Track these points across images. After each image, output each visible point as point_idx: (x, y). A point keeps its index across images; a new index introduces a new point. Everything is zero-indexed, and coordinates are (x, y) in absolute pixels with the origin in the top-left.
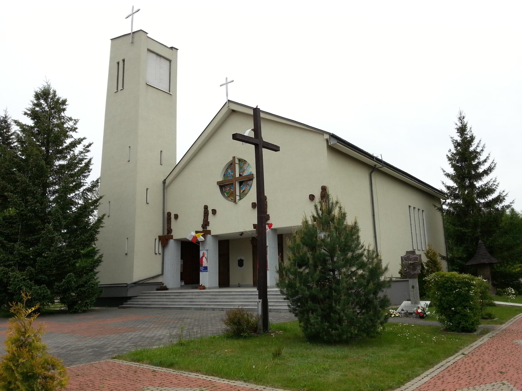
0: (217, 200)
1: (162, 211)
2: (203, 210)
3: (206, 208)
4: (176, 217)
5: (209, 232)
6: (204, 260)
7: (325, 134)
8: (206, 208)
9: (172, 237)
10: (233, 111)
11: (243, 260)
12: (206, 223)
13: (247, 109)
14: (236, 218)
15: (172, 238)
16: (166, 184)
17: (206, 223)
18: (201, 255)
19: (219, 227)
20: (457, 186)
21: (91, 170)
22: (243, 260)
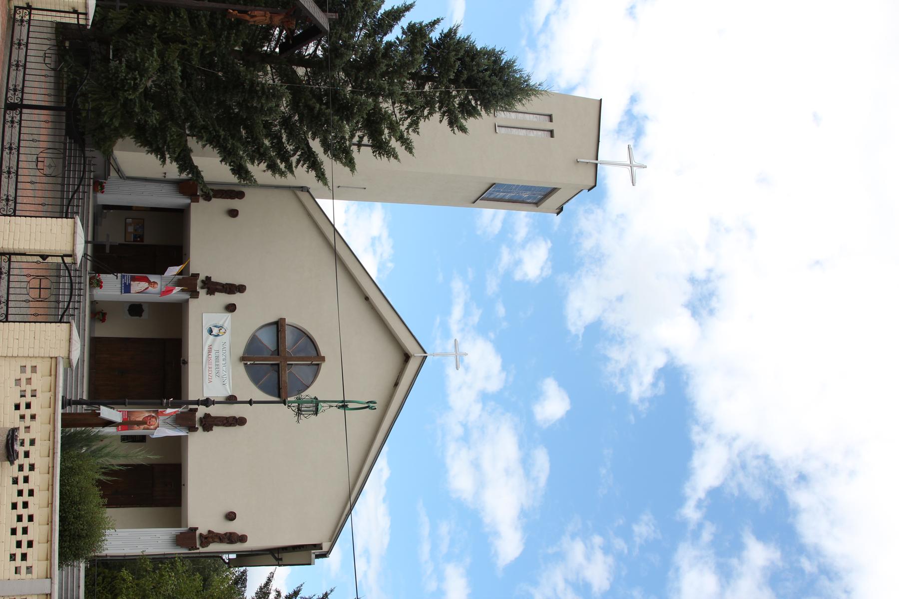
0: (253, 315)
1: (276, 386)
2: (237, 282)
3: (241, 289)
4: (233, 213)
5: (195, 294)
6: (144, 285)
7: (330, 544)
8: (241, 289)
9: (195, 198)
10: (407, 357)
11: (140, 316)
12: (212, 287)
13: (406, 388)
14: (214, 365)
15: (192, 201)
16: (300, 193)
17: (212, 287)
18: (152, 278)
19: (204, 313)
20: (189, 138)
21: (463, 129)
22: (140, 316)
